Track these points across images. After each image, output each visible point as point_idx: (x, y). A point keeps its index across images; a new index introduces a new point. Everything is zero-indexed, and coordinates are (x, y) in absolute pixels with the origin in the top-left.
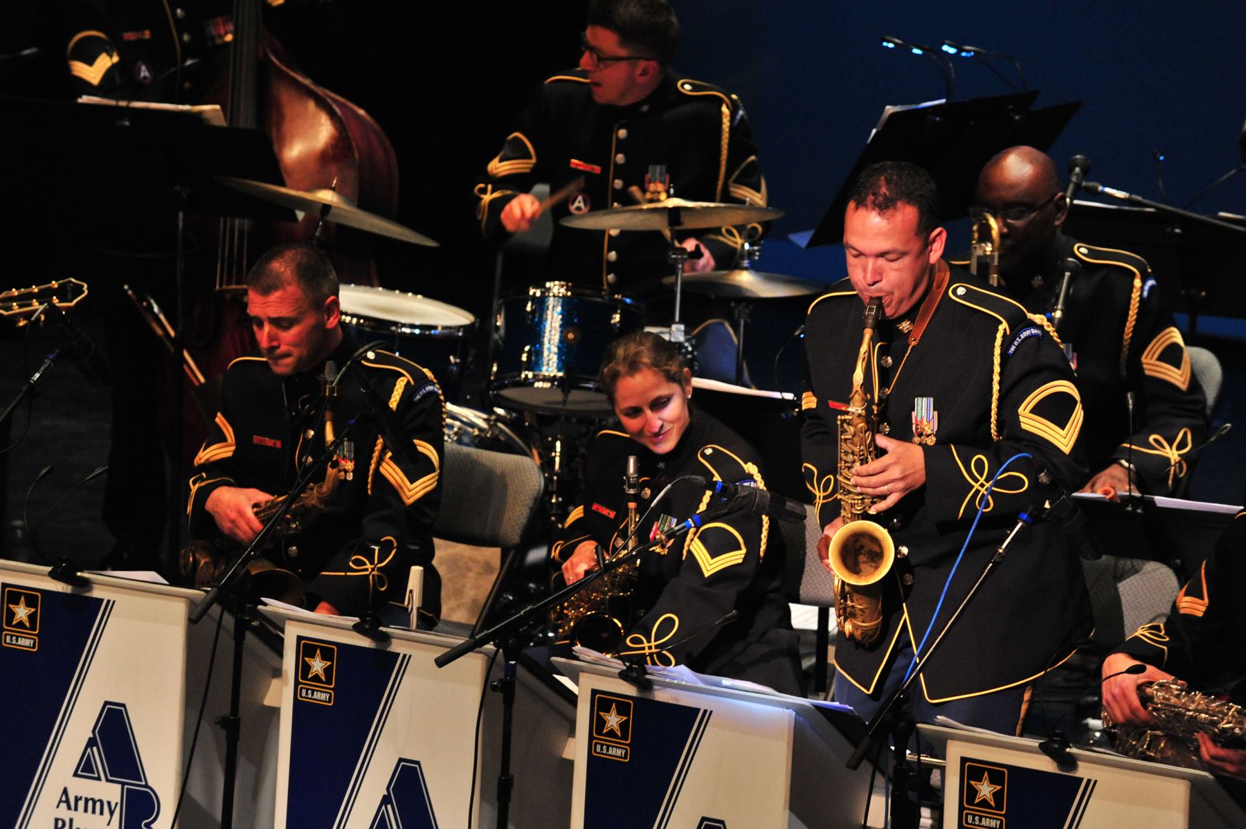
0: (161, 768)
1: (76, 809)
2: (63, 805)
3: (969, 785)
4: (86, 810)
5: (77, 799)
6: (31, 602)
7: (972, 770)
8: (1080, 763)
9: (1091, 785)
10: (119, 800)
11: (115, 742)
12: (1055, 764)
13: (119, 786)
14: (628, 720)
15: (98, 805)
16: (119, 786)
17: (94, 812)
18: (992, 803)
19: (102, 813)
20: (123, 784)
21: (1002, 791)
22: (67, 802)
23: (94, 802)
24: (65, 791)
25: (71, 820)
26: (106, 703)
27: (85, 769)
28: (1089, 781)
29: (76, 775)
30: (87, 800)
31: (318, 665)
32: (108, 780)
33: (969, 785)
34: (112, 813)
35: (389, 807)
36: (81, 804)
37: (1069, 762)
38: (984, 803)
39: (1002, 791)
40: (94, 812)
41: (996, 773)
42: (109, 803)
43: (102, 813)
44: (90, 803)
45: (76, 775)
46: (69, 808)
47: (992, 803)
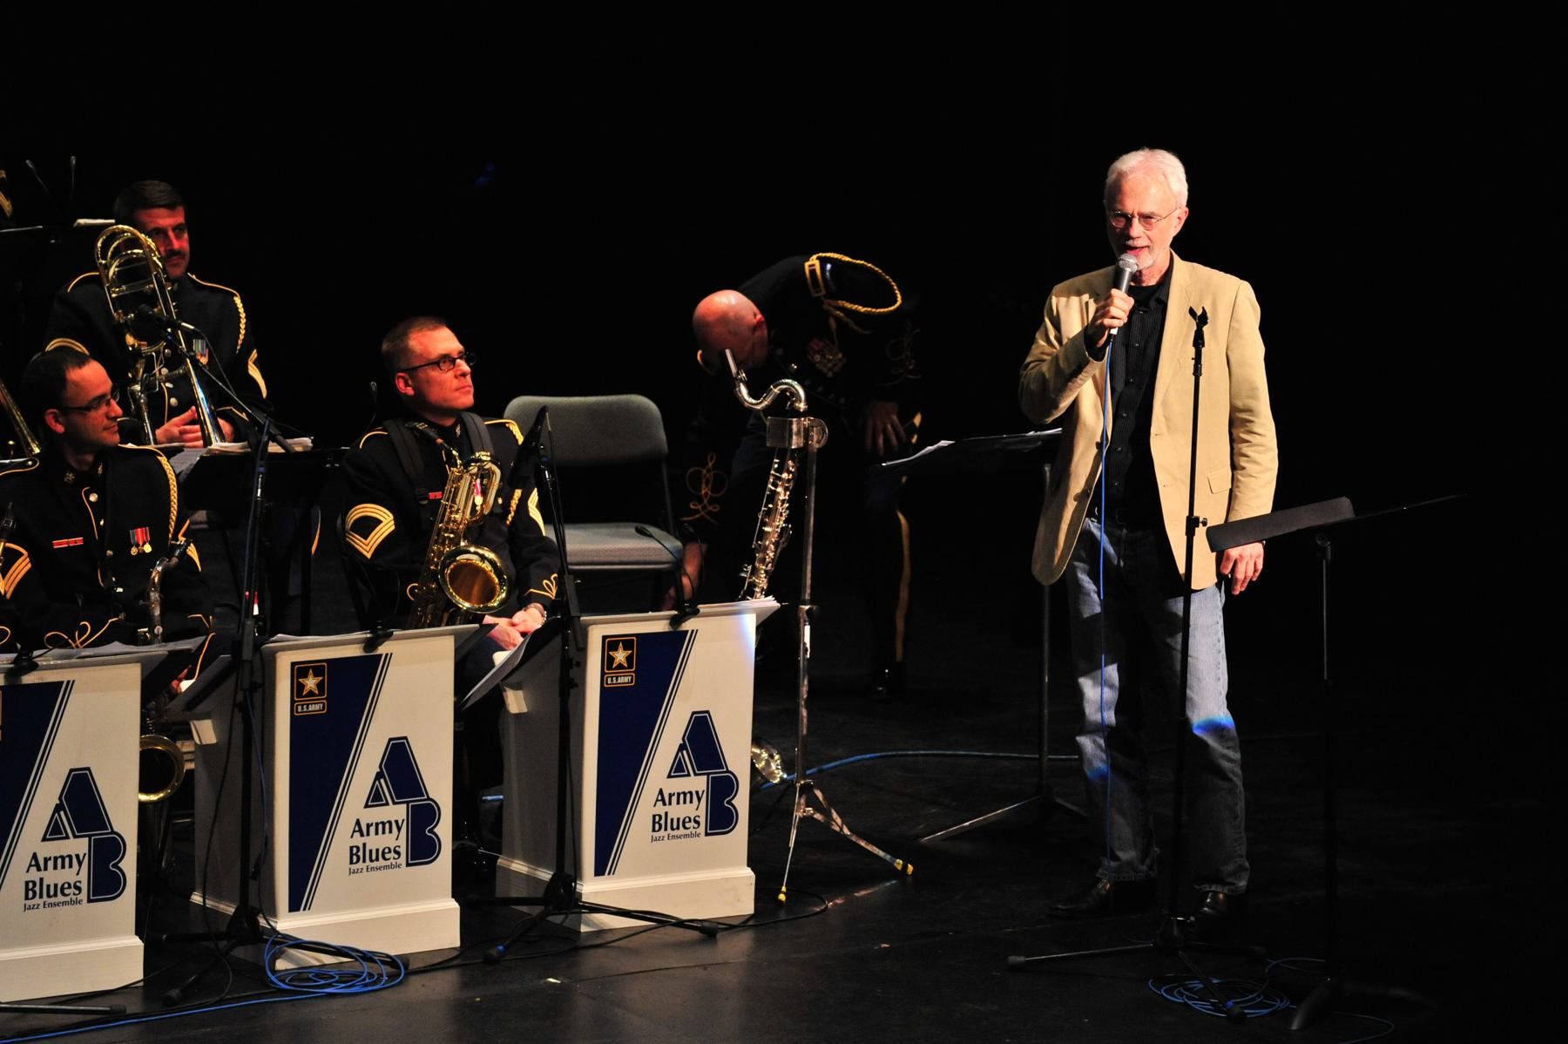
0: (439, 782)
9: (388, 657)
11: (701, 742)
22: (360, 831)
24: (661, 792)
34: (80, 864)
41: (317, 668)
46: (39, 869)
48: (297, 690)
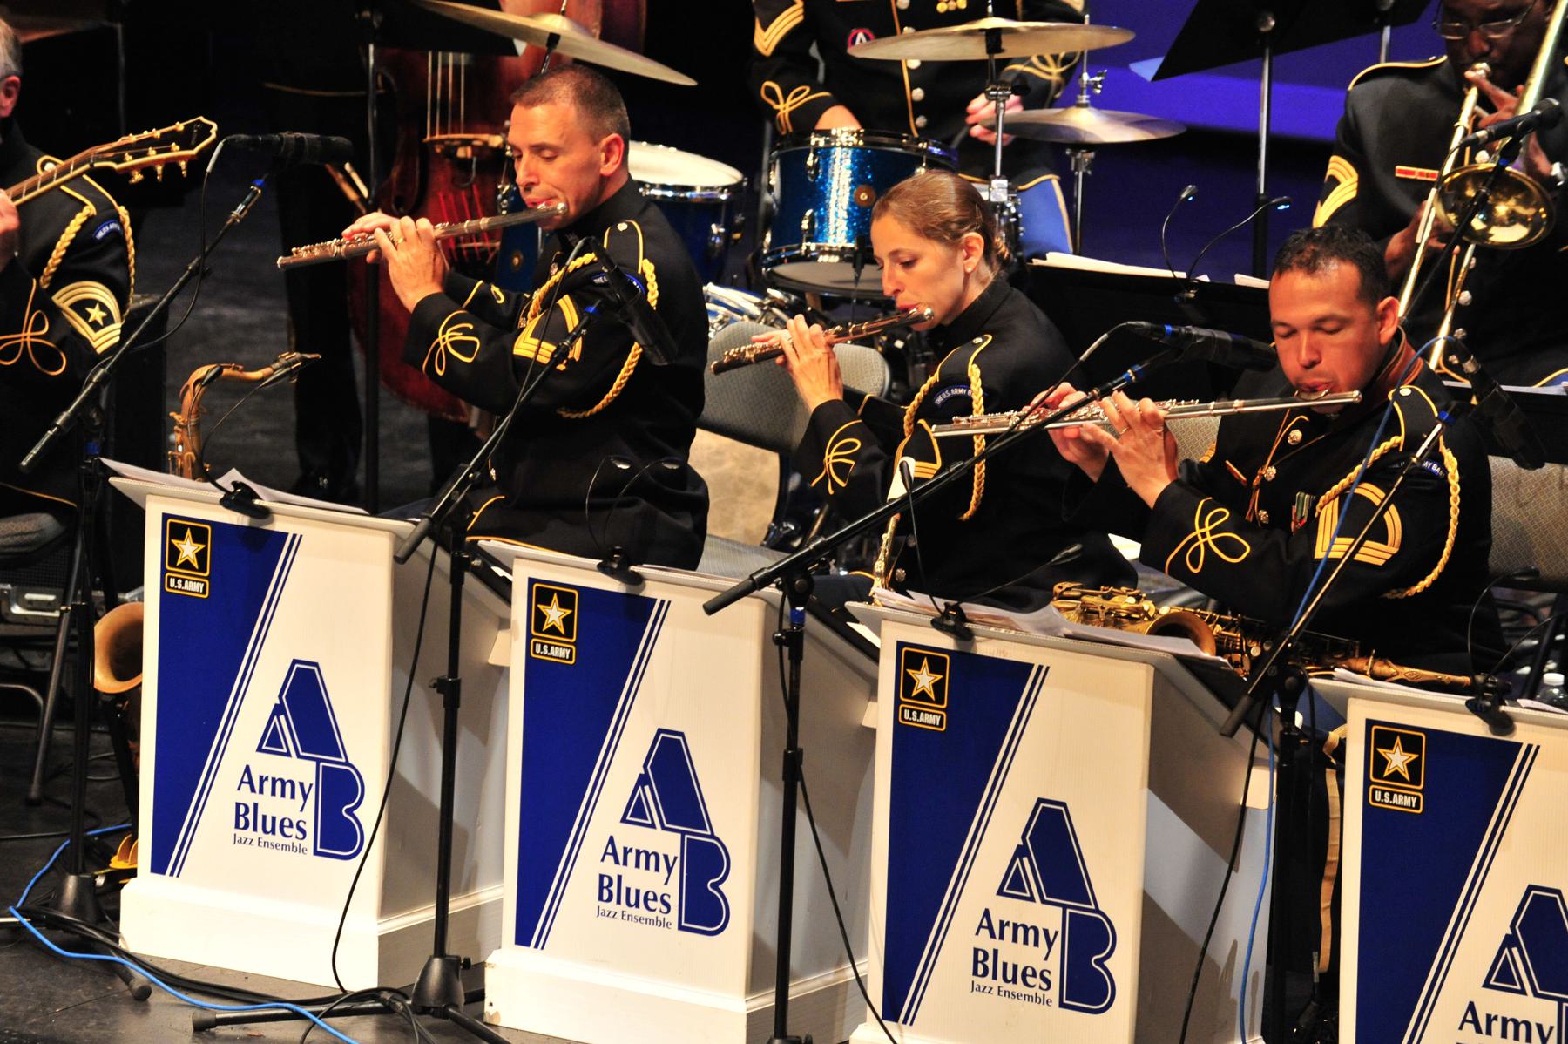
1: (1002, 937)
2: (985, 932)
3: (1376, 753)
4: (1015, 940)
5: (1490, 1019)
6: (1411, 744)
7: (1381, 736)
8: (1517, 725)
10: (1555, 1024)
12: (1487, 726)
13: (1555, 1004)
14: (1419, 759)
15: (288, 786)
16: (1555, 1004)
17: (1026, 942)
18: (1407, 777)
19: (1036, 944)
20: (1065, 907)
21: (1418, 760)
22: (1475, 1022)
23: (1517, 1024)
25: (996, 952)
26: (295, 662)
27: (1013, 885)
28: (1040, 667)
29: (1487, 985)
30: (1505, 1021)
31: (188, 549)
32: (1536, 995)
33: (1376, 753)
35: (1515, 950)
36: (1008, 931)
37: (1505, 724)
38: (923, 696)
39: (1418, 760)
40: (1026, 942)
41: (1410, 739)
42: (1540, 1027)
43: (1036, 944)
44: (643, 856)
45: (1487, 985)
46: (992, 935)
47: (1407, 777)
48: (1375, 765)
